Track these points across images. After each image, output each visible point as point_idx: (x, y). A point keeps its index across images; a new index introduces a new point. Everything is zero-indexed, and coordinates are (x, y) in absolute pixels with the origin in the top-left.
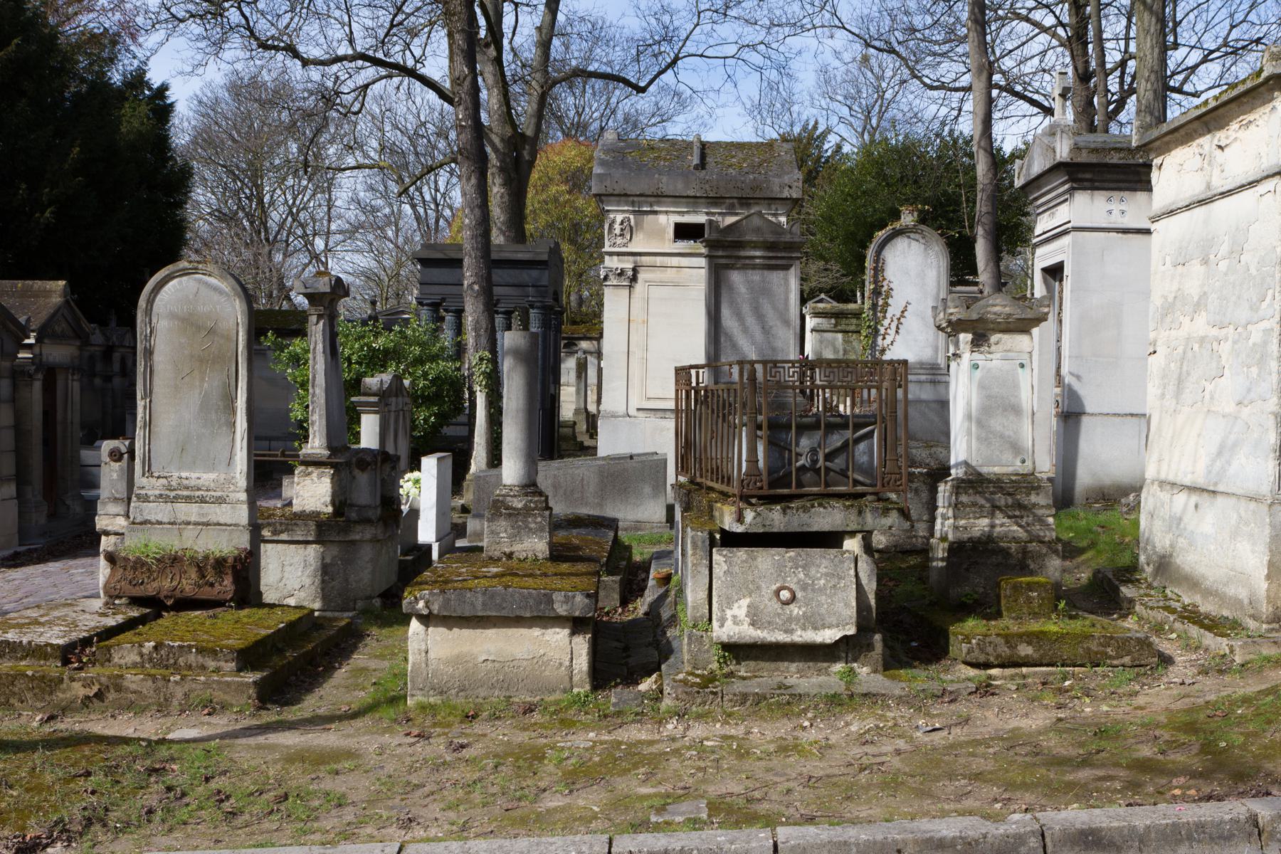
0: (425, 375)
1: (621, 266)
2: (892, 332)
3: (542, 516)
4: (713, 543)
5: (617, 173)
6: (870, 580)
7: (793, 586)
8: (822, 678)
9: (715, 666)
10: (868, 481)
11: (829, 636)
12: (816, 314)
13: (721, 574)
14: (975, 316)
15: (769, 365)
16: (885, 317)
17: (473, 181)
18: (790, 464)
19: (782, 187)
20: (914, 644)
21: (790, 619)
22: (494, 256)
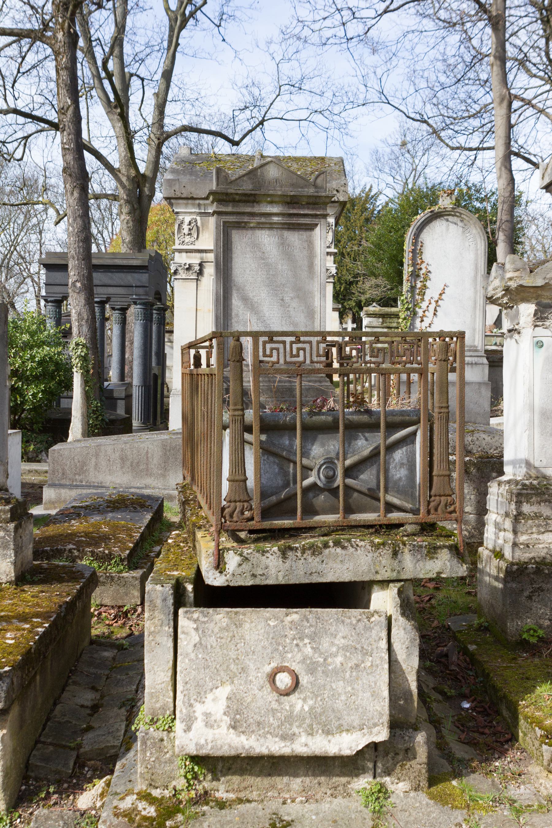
0: (32, 358)
1: (188, 262)
2: (430, 314)
4: (179, 600)
5: (185, 179)
6: (409, 655)
7: (295, 667)
8: (339, 801)
9: (181, 783)
10: (409, 506)
11: (347, 744)
12: (369, 315)
13: (190, 648)
14: (540, 282)
15: (262, 339)
16: (423, 300)
17: (76, 194)
18: (295, 482)
20: (466, 705)
21: (290, 718)
22: (95, 262)
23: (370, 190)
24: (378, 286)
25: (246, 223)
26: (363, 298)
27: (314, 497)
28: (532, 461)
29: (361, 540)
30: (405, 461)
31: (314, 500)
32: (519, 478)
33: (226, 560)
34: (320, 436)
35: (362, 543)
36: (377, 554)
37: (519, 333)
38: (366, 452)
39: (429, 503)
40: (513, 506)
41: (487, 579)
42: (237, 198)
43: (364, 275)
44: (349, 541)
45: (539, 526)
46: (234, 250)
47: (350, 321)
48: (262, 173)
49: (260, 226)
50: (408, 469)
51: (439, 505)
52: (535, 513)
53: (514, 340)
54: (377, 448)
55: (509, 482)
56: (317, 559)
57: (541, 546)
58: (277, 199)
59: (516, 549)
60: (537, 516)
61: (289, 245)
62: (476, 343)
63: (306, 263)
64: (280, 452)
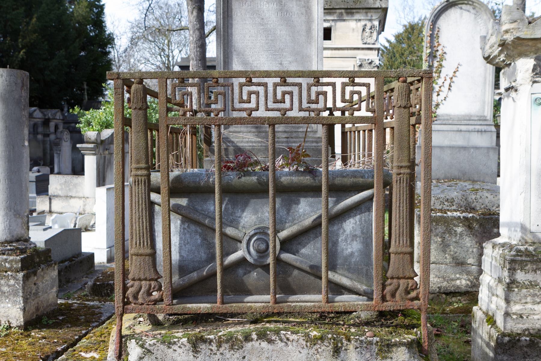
2: (445, 89)
3: (15, 278)
10: (362, 287)
16: (439, 77)
17: (195, 13)
22: (208, 64)
27: (245, 274)
28: (528, 226)
29: (293, 333)
30: (358, 232)
31: (245, 278)
32: (514, 242)
33: (129, 350)
34: (253, 201)
35: (295, 337)
36: (313, 351)
37: (516, 90)
38: (308, 222)
39: (384, 287)
40: (506, 273)
41: (480, 341)
44: (277, 332)
45: (534, 295)
46: (234, 17)
50: (363, 243)
51: (396, 290)
52: (530, 282)
53: (511, 99)
54: (320, 217)
55: (503, 245)
56: (237, 355)
57: (536, 317)
59: (508, 319)
60: (532, 285)
61: (287, 11)
62: (486, 114)
63: (304, 28)
64: (202, 220)
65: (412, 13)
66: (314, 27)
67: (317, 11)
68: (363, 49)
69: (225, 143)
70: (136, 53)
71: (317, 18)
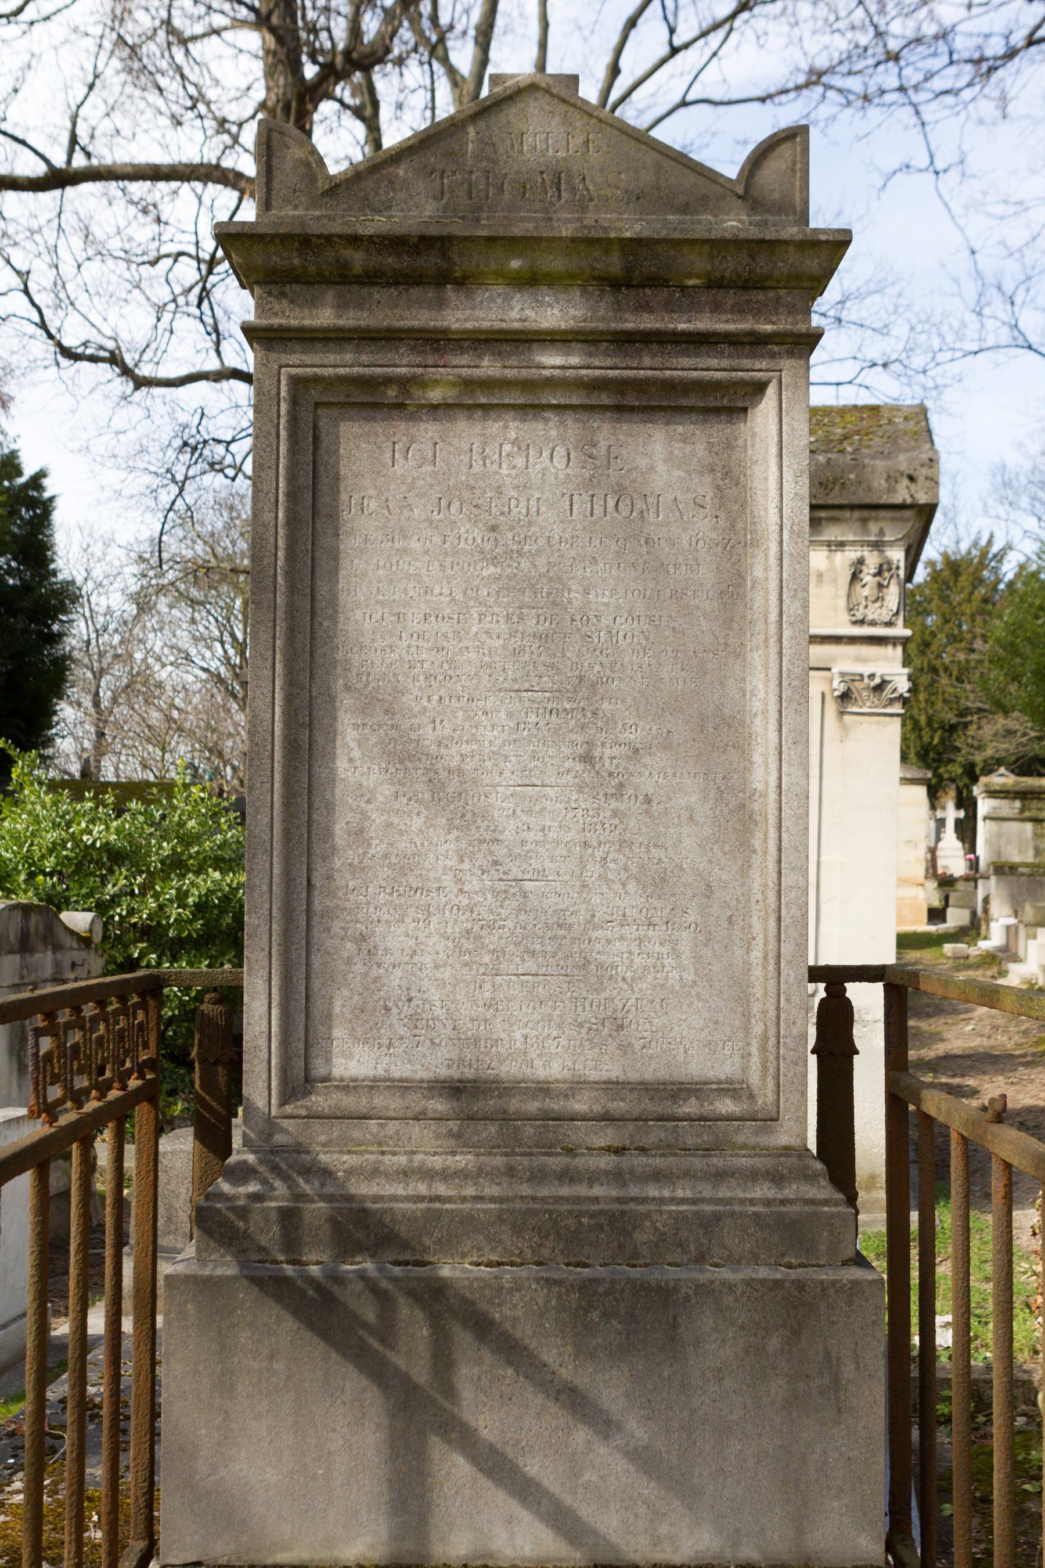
0: (181, 897)
12: (992, 793)
19: (892, 479)
23: (990, 542)
24: (1009, 733)
25: (404, 383)
26: (978, 758)
42: (358, 259)
43: (980, 710)
46: (349, 516)
47: (951, 805)
48: (486, 143)
49: (476, 400)
58: (555, 263)
65: (951, 527)
66: (758, 572)
67: (773, 493)
68: (853, 640)
69: (286, 1178)
70: (151, 635)
71: (774, 528)
